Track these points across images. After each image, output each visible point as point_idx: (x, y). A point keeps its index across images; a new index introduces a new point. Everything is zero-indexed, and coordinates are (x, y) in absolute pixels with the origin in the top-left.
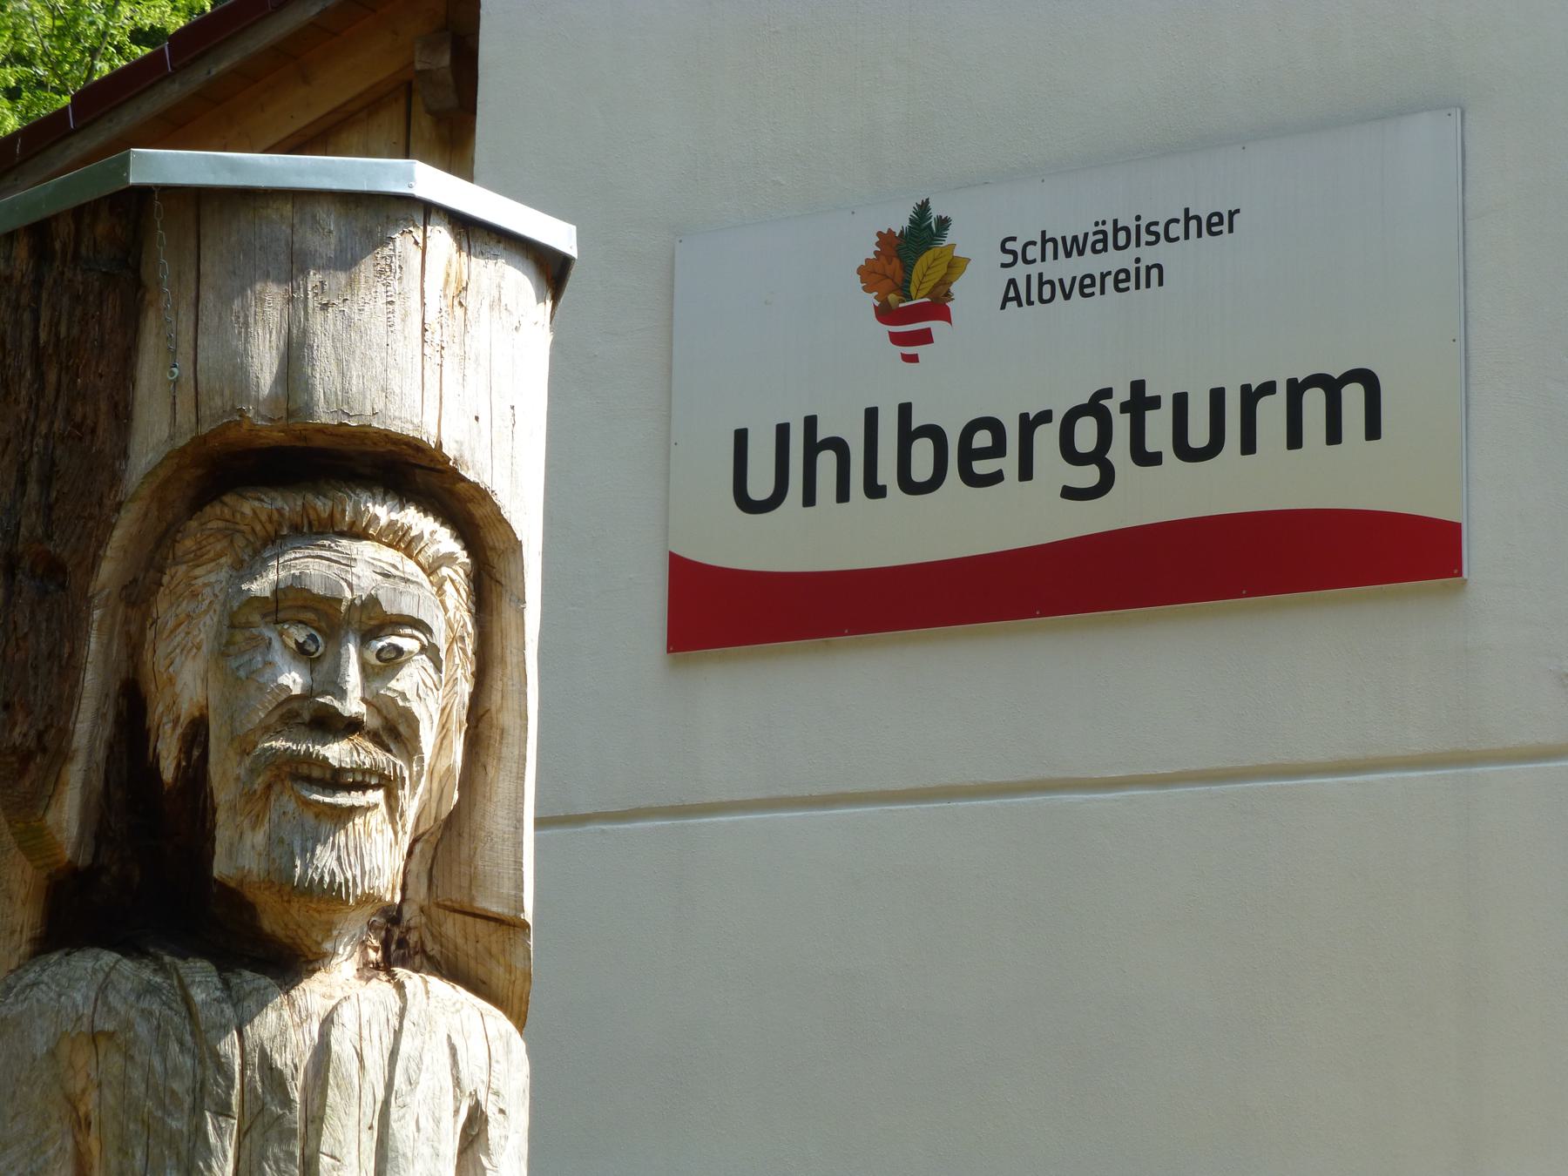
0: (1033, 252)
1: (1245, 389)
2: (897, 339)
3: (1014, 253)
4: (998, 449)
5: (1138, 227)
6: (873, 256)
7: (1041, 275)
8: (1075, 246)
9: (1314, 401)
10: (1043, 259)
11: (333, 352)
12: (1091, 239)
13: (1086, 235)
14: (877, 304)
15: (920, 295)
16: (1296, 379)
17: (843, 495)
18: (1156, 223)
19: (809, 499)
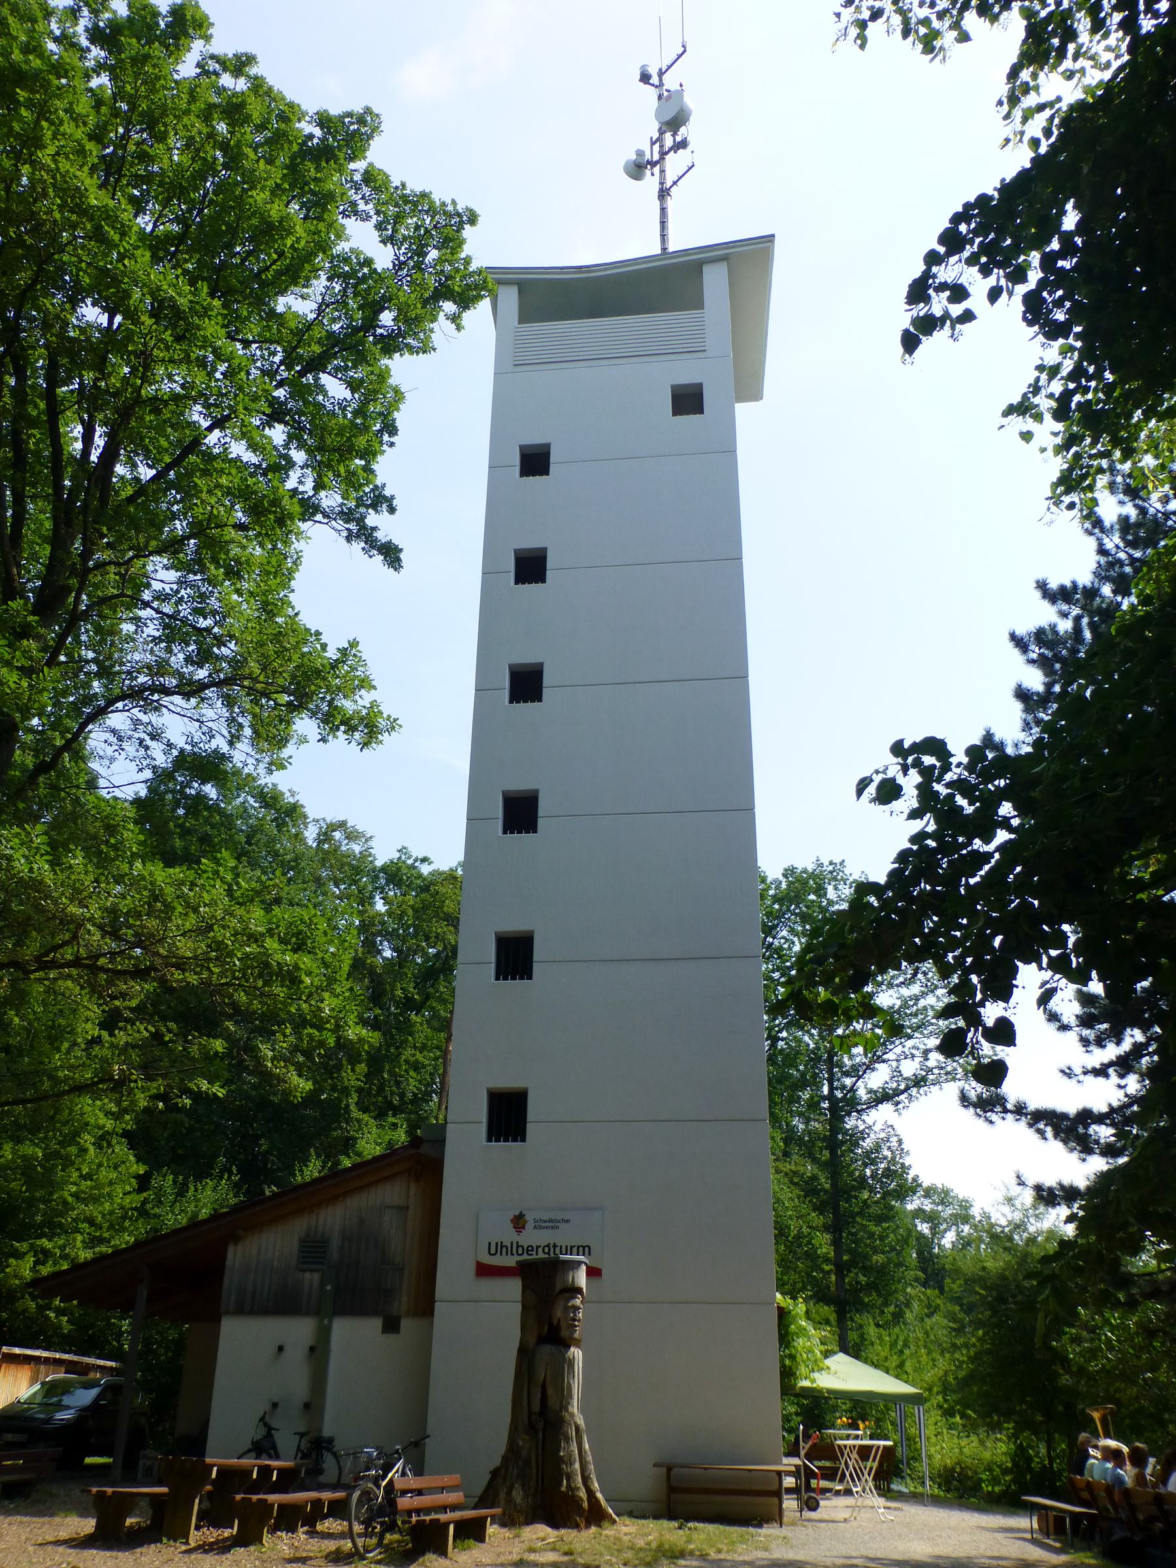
11: (330, 1525)
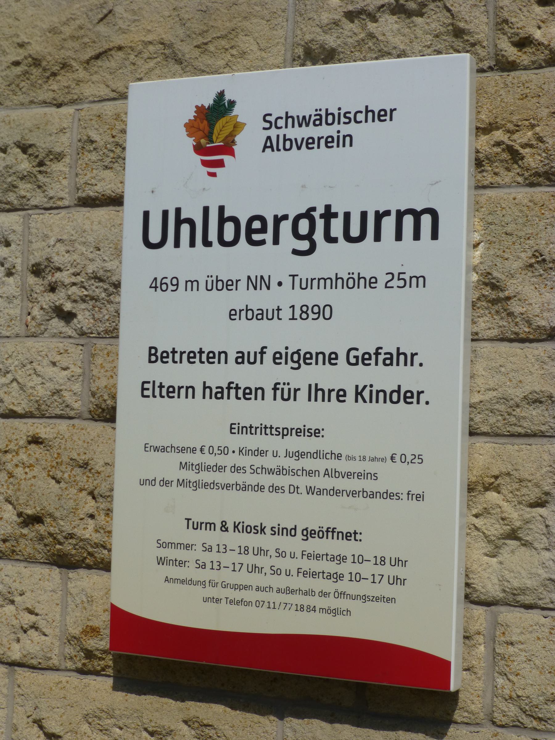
0: (281, 123)
1: (377, 212)
2: (205, 163)
3: (270, 122)
4: (263, 230)
5: (339, 114)
6: (193, 118)
7: (285, 136)
8: (304, 121)
9: (408, 220)
10: (286, 127)
12: (313, 118)
13: (310, 116)
14: (195, 144)
15: (218, 140)
16: (400, 210)
17: (192, 244)
18: (350, 113)
19: (177, 244)
